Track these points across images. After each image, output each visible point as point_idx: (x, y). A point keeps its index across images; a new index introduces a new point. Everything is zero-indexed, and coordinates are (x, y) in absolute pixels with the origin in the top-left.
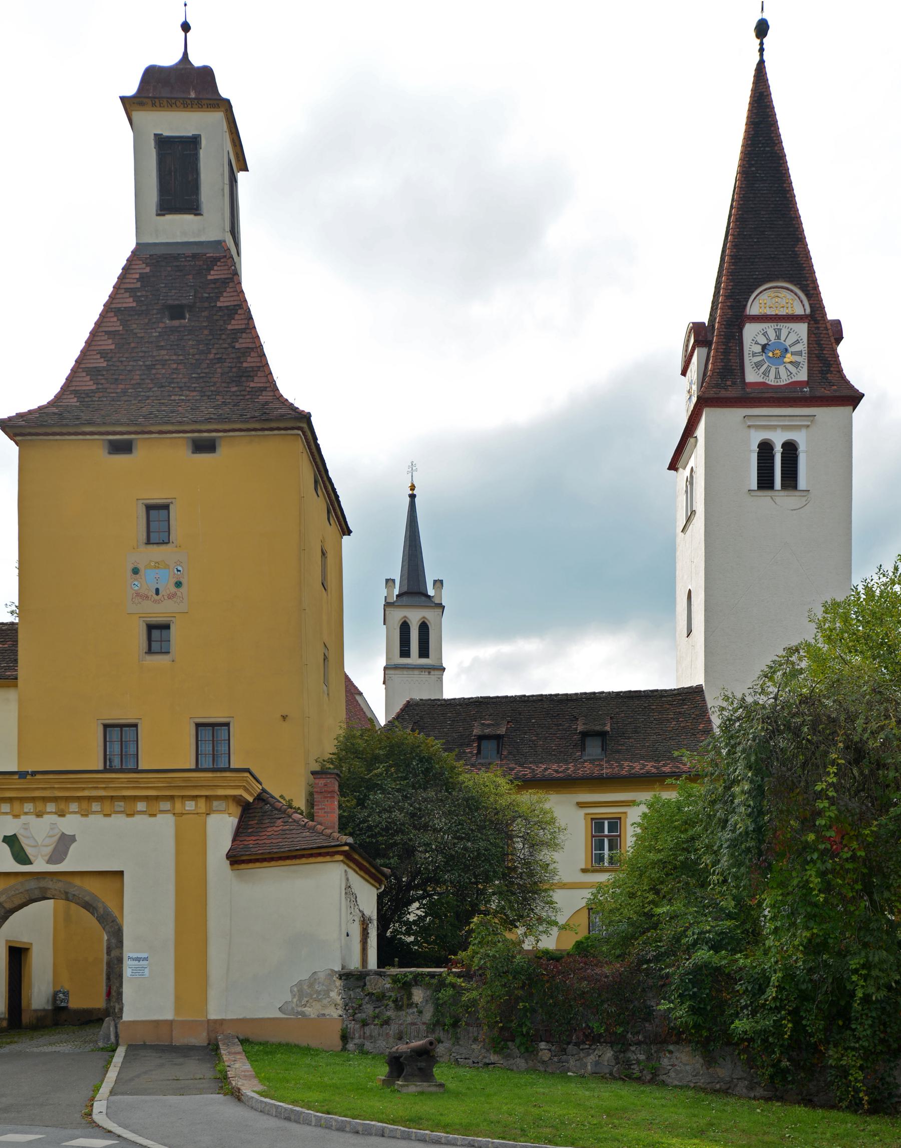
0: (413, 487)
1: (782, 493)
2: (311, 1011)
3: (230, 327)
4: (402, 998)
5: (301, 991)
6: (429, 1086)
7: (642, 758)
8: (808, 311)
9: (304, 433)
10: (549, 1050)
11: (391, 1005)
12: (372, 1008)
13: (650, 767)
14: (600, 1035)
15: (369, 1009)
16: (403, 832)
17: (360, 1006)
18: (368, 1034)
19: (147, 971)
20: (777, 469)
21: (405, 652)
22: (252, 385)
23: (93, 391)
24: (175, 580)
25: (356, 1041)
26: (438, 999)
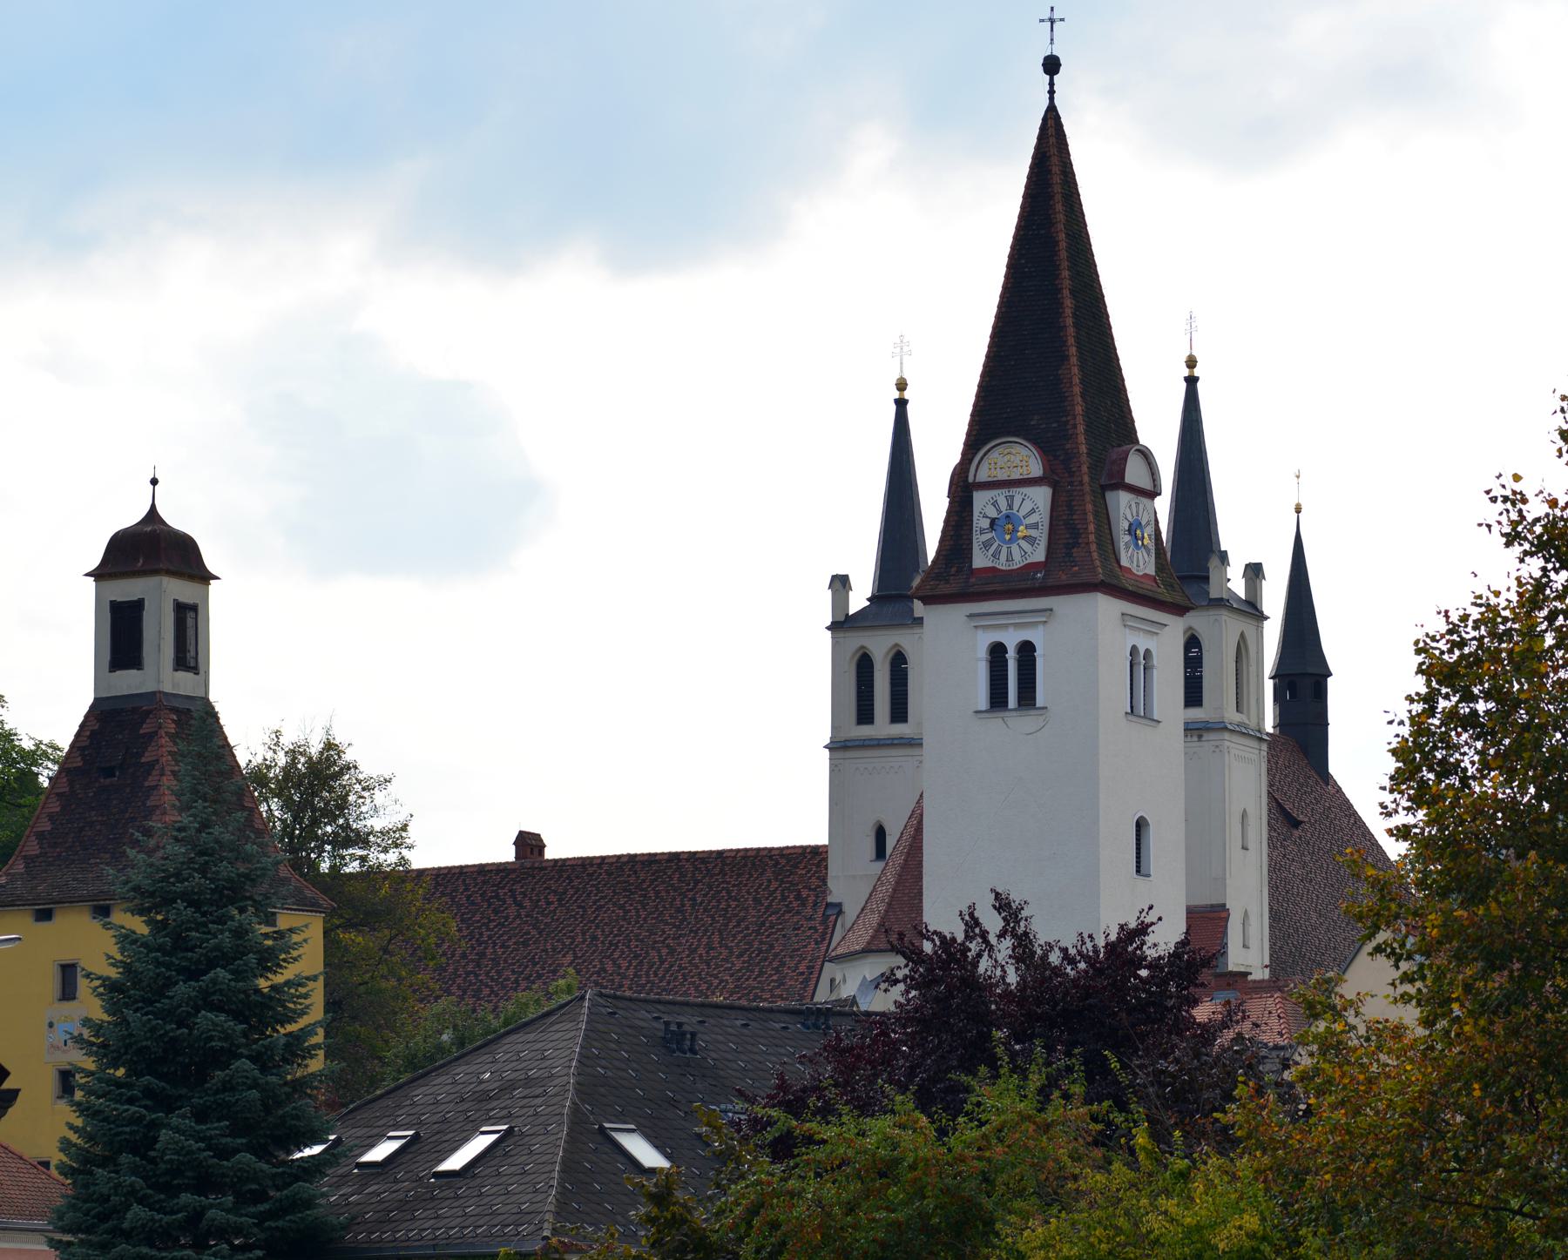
21: (865, 714)
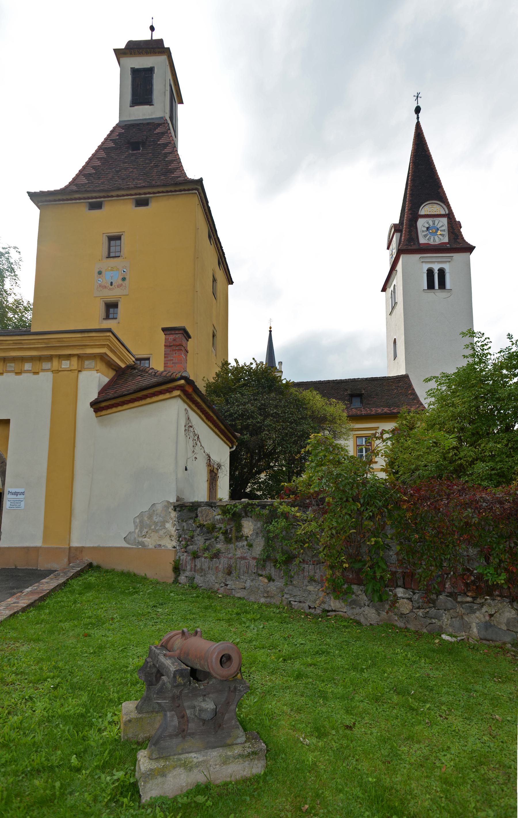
0: (271, 328)
1: (439, 291)
2: (150, 542)
3: (166, 159)
4: (231, 530)
5: (141, 522)
6: (225, 762)
7: (382, 406)
8: (447, 212)
9: (199, 193)
10: (410, 599)
11: (222, 537)
12: (203, 540)
13: (386, 410)
14: (497, 586)
15: (200, 542)
16: (253, 417)
17: (192, 537)
18: (198, 566)
19: (23, 504)
20: (436, 281)
22: (173, 175)
23: (86, 184)
24: (122, 277)
25: (188, 573)
26: (269, 531)
